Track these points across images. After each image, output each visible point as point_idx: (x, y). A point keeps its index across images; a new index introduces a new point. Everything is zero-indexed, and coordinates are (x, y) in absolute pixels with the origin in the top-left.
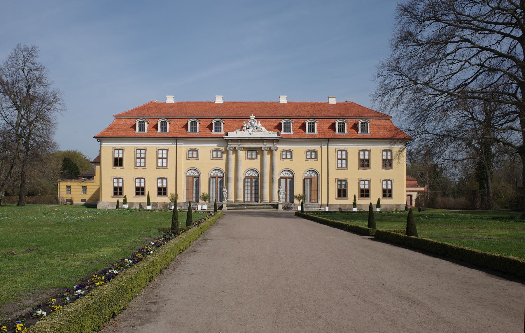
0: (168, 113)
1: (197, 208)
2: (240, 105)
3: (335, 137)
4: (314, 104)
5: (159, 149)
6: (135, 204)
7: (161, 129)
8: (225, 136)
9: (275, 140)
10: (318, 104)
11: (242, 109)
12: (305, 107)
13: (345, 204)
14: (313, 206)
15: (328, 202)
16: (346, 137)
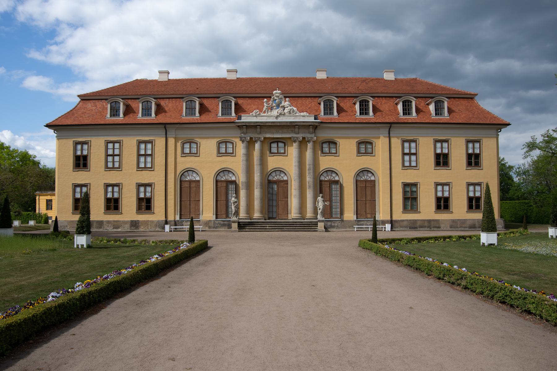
1: (385, 228)
3: (400, 121)
5: (108, 143)
6: (105, 223)
7: (411, 112)
8: (237, 121)
9: (311, 126)
10: (370, 80)
13: (415, 220)
14: (368, 224)
15: (391, 217)
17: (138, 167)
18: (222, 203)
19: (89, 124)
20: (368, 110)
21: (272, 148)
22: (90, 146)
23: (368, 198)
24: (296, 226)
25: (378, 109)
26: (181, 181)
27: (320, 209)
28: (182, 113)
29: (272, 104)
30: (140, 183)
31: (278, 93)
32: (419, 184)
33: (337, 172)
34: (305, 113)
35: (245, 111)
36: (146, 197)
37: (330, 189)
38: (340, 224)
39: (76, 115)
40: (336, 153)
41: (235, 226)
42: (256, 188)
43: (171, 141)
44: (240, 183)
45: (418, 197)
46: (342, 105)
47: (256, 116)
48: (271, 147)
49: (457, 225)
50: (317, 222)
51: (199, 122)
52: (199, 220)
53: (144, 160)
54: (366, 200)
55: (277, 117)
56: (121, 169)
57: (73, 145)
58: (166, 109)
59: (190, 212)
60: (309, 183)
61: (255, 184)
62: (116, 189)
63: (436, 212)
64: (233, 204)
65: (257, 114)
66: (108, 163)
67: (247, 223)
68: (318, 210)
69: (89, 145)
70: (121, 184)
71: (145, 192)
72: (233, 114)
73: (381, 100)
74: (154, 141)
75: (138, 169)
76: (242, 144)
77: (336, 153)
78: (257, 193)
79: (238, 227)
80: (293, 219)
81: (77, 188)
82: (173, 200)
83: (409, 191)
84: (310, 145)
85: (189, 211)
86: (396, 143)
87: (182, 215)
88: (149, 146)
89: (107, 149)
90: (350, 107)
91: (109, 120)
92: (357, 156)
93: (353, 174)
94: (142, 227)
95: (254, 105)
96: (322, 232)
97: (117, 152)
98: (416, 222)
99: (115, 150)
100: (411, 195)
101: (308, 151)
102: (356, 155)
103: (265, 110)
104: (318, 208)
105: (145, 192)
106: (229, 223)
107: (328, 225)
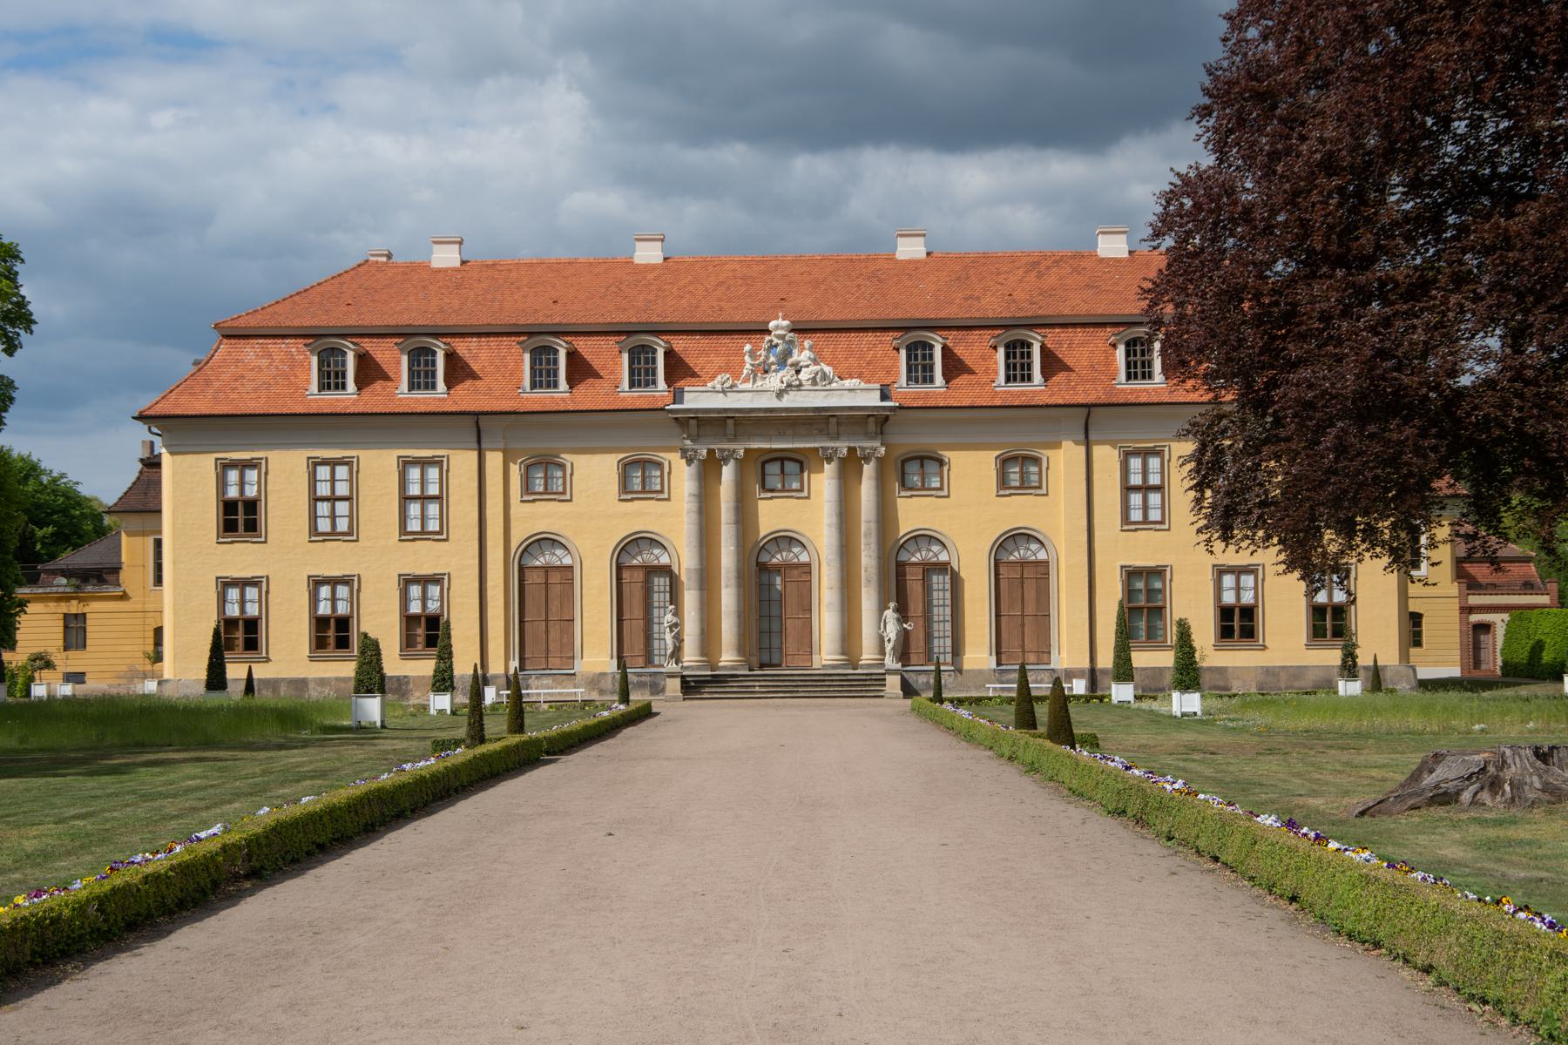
0: (442, 310)
2: (734, 270)
3: (1114, 400)
4: (1038, 263)
5: (316, 464)
6: (311, 685)
10: (1055, 261)
11: (743, 289)
12: (999, 274)
13: (1159, 668)
15: (1092, 659)
16: (1156, 400)
17: (403, 529)
18: (634, 627)
19: (262, 412)
20: (1029, 369)
21: (767, 477)
22: (266, 473)
23: (1030, 610)
24: (830, 686)
25: (1060, 361)
26: (521, 569)
27: (889, 641)
28: (521, 379)
29: (767, 357)
30: (409, 575)
31: (783, 328)
32: (1168, 569)
33: (943, 539)
34: (854, 380)
35: (694, 375)
36: (427, 611)
37: (927, 589)
38: (952, 679)
39: (217, 384)
40: (941, 489)
41: (674, 685)
42: (727, 586)
43: (494, 460)
44: (683, 571)
45: (1168, 606)
46: (959, 351)
47: (724, 392)
48: (763, 474)
49: (1279, 681)
50: (884, 674)
51: (571, 408)
52: (572, 672)
53: (418, 513)
54: (1022, 615)
55: (780, 394)
56: (355, 538)
57: (216, 469)
58: (475, 367)
59: (547, 651)
60: (866, 571)
61: (723, 576)
62: (342, 591)
63: (1217, 648)
64: (668, 630)
65: (727, 385)
66: (319, 519)
67: (709, 678)
68: (886, 643)
69: (263, 470)
70: (356, 578)
71: (424, 599)
72: (661, 383)
73: (1072, 335)
74: (445, 459)
75: (403, 537)
76: (686, 467)
77: (941, 489)
78: (728, 598)
79: (682, 688)
80: (824, 667)
81: (230, 590)
82: (503, 618)
83: (1140, 590)
84: (868, 470)
85: (544, 648)
86: (1106, 457)
87: (527, 661)
88: (433, 473)
89: (313, 481)
90: (984, 358)
91: (315, 400)
92: (997, 496)
93: (986, 544)
94: (417, 694)
95: (717, 355)
96: (896, 698)
97: (342, 489)
98: (1161, 674)
99: (337, 484)
100: (1148, 601)
101: (864, 482)
102: (995, 493)
103: (748, 375)
104: (886, 639)
105: (424, 599)
106: (653, 679)
107: (920, 681)
